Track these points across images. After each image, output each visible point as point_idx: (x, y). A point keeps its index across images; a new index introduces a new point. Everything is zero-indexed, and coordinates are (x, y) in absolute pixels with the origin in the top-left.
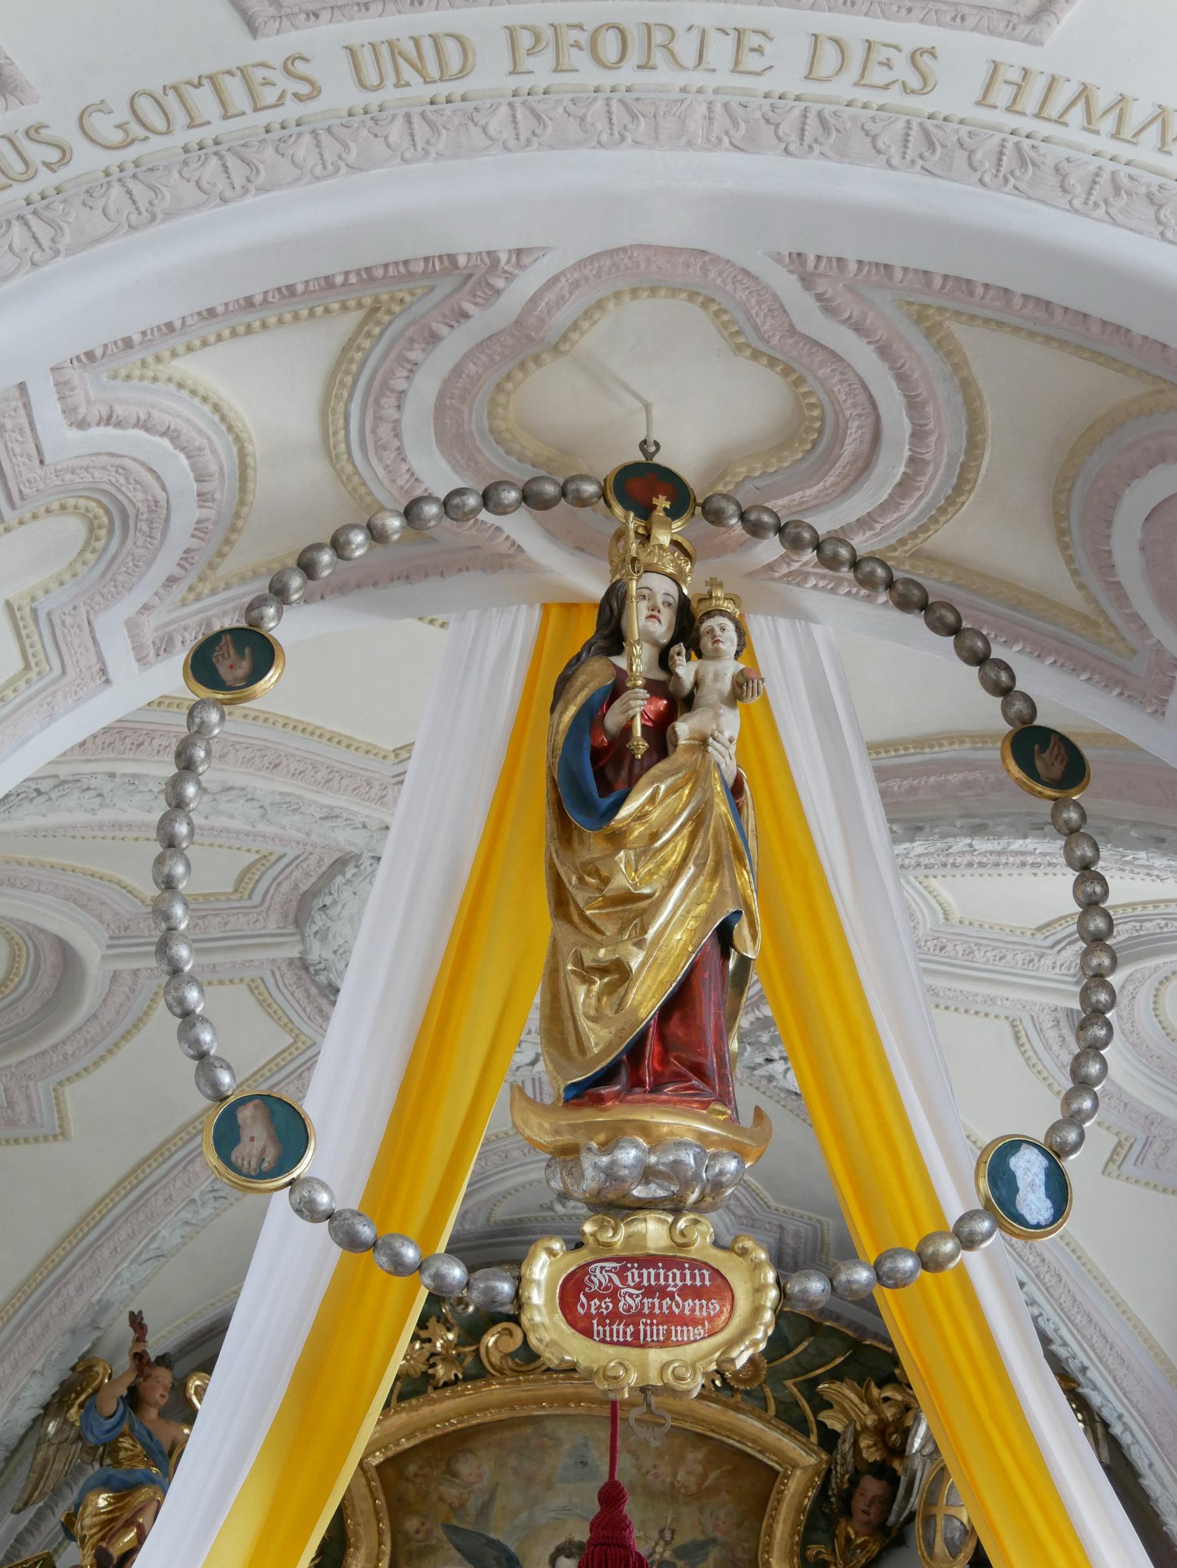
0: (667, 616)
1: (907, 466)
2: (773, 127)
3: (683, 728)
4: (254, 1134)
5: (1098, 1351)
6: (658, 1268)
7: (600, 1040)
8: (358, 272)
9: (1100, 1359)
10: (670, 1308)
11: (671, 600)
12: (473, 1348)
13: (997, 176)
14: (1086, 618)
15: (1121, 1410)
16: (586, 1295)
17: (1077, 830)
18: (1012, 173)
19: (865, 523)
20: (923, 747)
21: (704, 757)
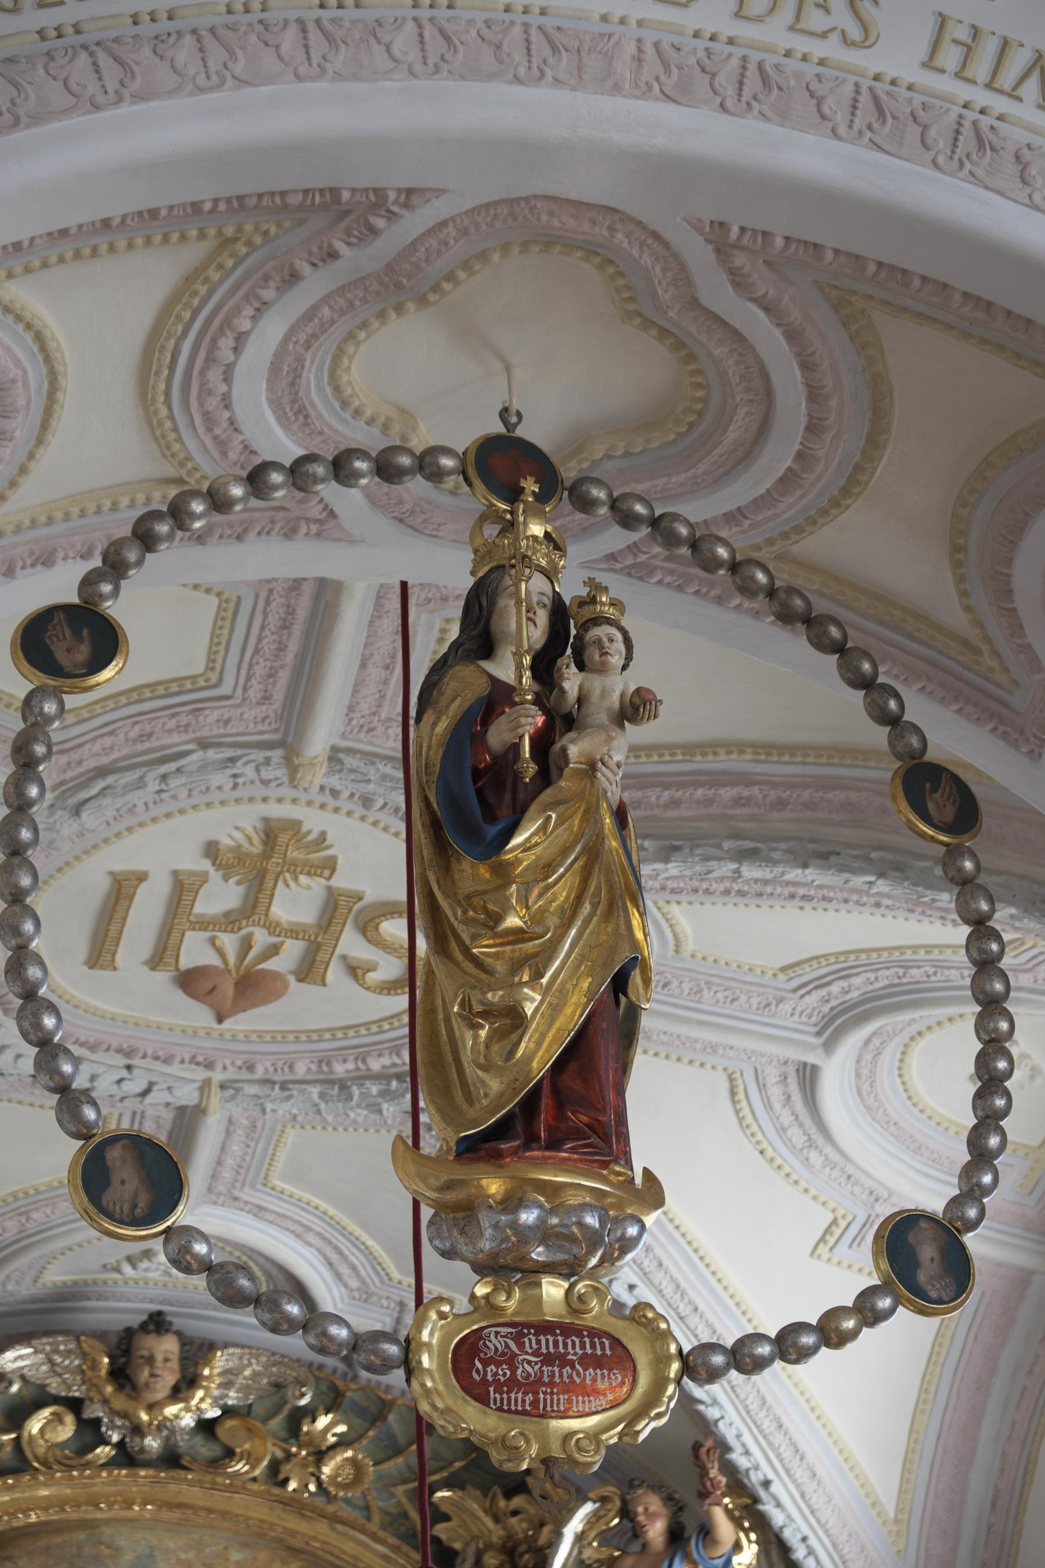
0: (542, 617)
1: (793, 461)
2: (708, 77)
3: (576, 749)
4: (125, 1176)
5: (786, 1461)
6: (556, 1335)
7: (493, 1092)
8: (229, 201)
9: (787, 1471)
10: (570, 1376)
11: (546, 600)
12: (13, 1436)
13: (951, 158)
14: (966, 644)
15: (806, 1531)
16: (481, 1360)
17: (971, 881)
18: (968, 156)
19: (731, 518)
20: (693, 754)
21: (592, 783)
